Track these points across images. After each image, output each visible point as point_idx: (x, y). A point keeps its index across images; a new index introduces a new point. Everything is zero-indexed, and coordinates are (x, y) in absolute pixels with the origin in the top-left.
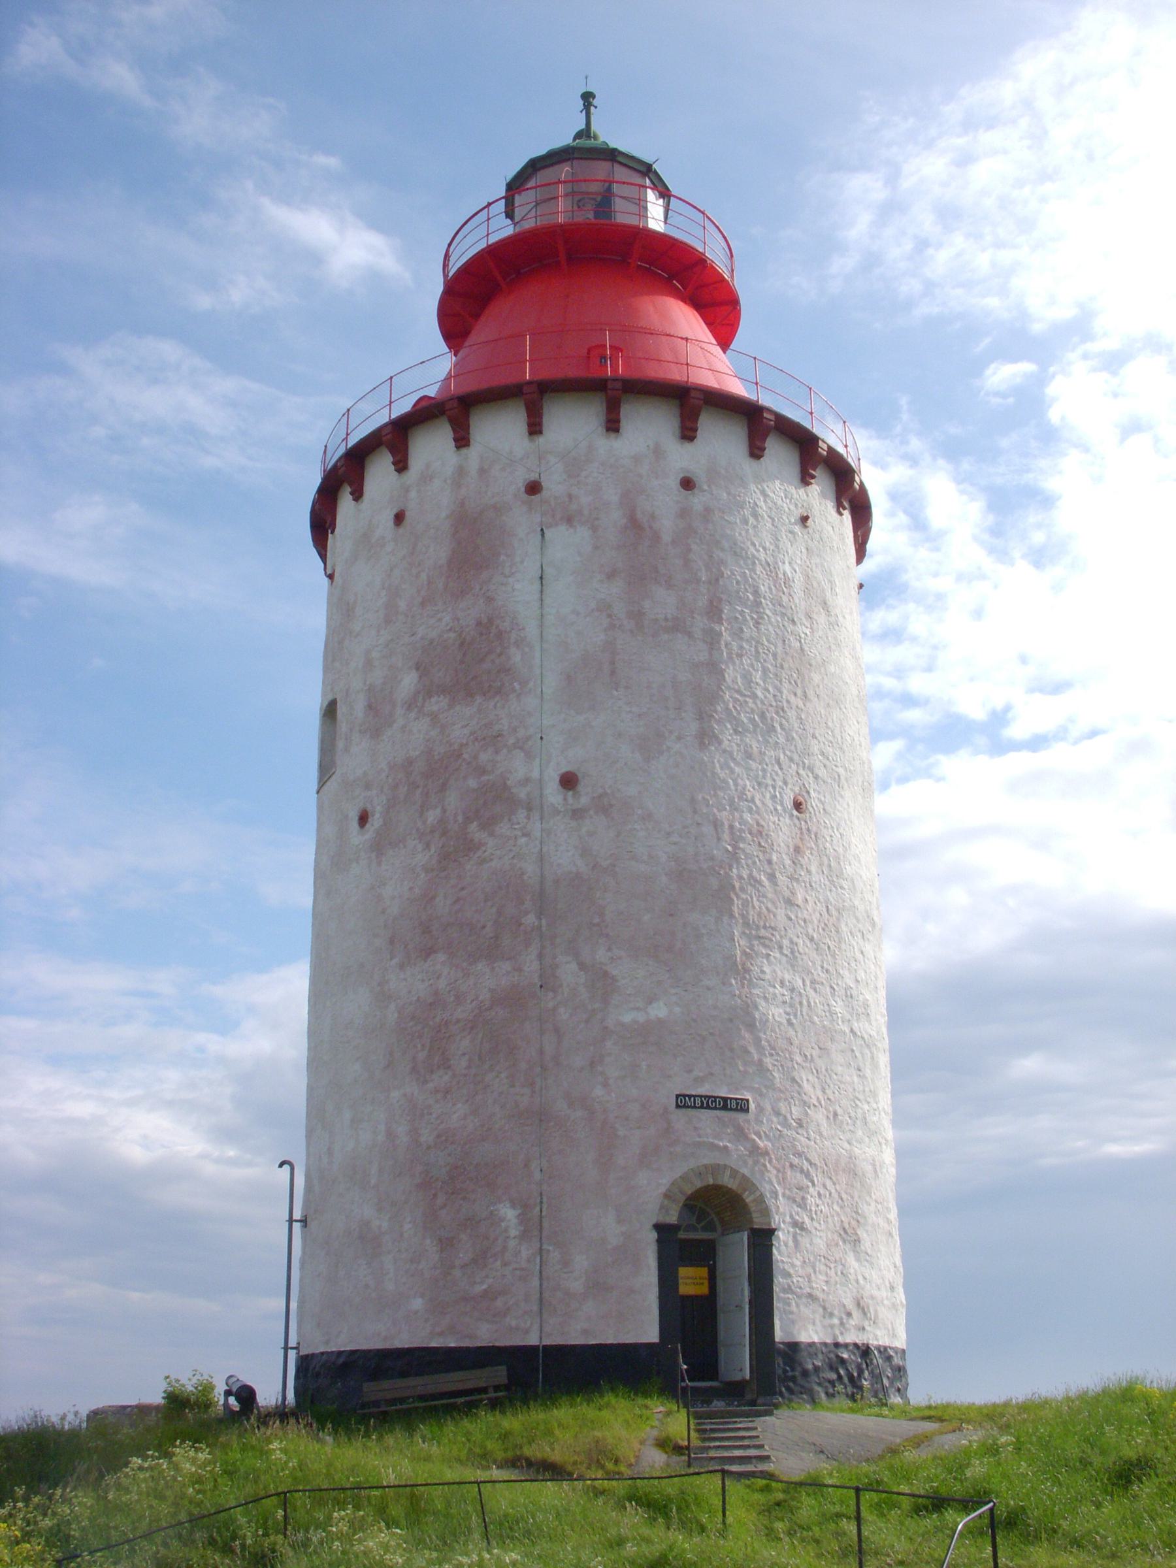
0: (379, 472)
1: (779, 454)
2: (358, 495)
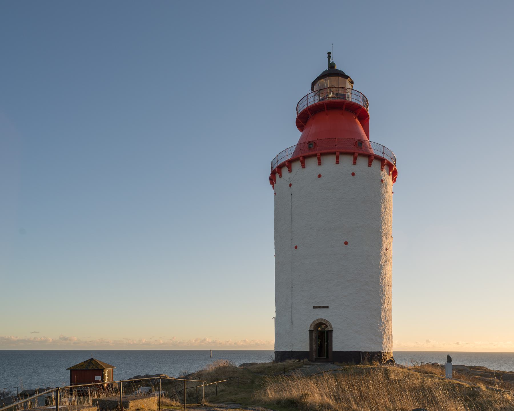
0: (285, 171)
1: (376, 164)
2: (281, 176)
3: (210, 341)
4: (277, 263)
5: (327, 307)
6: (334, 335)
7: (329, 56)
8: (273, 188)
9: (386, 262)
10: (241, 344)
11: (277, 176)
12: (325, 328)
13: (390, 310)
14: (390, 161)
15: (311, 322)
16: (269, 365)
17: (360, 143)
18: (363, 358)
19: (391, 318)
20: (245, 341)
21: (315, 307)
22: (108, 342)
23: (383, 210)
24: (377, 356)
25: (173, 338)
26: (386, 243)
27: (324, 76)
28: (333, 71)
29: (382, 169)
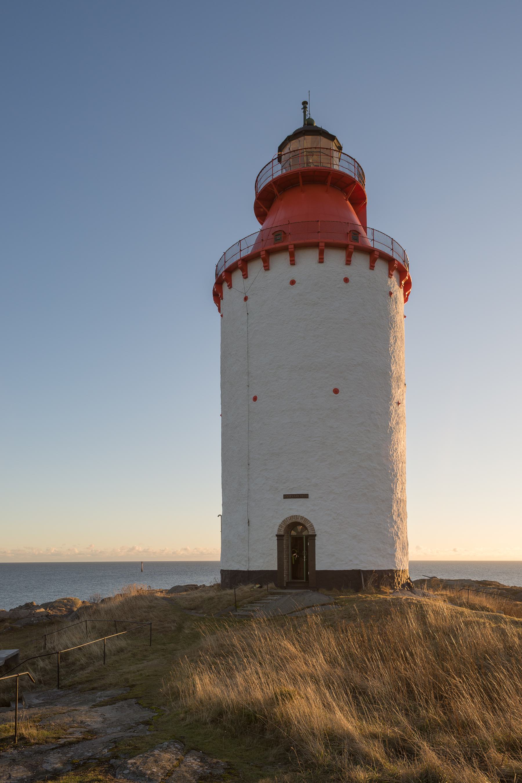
0: (237, 277)
1: (381, 266)
2: (230, 286)
3: (141, 550)
4: (224, 426)
5: (306, 496)
6: (318, 542)
7: (305, 108)
8: (219, 310)
9: (397, 423)
10: (182, 553)
11: (225, 285)
12: (302, 531)
13: (404, 501)
14: (402, 263)
15: (280, 521)
16: (212, 594)
17: (356, 234)
18: (365, 581)
19: (406, 514)
20: (186, 549)
21: (286, 497)
22: (5, 552)
23: (392, 341)
24: (386, 577)
25: (91, 546)
26: (398, 393)
27: (297, 135)
28: (309, 129)
29: (390, 276)
